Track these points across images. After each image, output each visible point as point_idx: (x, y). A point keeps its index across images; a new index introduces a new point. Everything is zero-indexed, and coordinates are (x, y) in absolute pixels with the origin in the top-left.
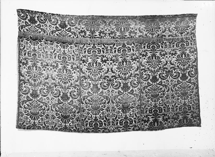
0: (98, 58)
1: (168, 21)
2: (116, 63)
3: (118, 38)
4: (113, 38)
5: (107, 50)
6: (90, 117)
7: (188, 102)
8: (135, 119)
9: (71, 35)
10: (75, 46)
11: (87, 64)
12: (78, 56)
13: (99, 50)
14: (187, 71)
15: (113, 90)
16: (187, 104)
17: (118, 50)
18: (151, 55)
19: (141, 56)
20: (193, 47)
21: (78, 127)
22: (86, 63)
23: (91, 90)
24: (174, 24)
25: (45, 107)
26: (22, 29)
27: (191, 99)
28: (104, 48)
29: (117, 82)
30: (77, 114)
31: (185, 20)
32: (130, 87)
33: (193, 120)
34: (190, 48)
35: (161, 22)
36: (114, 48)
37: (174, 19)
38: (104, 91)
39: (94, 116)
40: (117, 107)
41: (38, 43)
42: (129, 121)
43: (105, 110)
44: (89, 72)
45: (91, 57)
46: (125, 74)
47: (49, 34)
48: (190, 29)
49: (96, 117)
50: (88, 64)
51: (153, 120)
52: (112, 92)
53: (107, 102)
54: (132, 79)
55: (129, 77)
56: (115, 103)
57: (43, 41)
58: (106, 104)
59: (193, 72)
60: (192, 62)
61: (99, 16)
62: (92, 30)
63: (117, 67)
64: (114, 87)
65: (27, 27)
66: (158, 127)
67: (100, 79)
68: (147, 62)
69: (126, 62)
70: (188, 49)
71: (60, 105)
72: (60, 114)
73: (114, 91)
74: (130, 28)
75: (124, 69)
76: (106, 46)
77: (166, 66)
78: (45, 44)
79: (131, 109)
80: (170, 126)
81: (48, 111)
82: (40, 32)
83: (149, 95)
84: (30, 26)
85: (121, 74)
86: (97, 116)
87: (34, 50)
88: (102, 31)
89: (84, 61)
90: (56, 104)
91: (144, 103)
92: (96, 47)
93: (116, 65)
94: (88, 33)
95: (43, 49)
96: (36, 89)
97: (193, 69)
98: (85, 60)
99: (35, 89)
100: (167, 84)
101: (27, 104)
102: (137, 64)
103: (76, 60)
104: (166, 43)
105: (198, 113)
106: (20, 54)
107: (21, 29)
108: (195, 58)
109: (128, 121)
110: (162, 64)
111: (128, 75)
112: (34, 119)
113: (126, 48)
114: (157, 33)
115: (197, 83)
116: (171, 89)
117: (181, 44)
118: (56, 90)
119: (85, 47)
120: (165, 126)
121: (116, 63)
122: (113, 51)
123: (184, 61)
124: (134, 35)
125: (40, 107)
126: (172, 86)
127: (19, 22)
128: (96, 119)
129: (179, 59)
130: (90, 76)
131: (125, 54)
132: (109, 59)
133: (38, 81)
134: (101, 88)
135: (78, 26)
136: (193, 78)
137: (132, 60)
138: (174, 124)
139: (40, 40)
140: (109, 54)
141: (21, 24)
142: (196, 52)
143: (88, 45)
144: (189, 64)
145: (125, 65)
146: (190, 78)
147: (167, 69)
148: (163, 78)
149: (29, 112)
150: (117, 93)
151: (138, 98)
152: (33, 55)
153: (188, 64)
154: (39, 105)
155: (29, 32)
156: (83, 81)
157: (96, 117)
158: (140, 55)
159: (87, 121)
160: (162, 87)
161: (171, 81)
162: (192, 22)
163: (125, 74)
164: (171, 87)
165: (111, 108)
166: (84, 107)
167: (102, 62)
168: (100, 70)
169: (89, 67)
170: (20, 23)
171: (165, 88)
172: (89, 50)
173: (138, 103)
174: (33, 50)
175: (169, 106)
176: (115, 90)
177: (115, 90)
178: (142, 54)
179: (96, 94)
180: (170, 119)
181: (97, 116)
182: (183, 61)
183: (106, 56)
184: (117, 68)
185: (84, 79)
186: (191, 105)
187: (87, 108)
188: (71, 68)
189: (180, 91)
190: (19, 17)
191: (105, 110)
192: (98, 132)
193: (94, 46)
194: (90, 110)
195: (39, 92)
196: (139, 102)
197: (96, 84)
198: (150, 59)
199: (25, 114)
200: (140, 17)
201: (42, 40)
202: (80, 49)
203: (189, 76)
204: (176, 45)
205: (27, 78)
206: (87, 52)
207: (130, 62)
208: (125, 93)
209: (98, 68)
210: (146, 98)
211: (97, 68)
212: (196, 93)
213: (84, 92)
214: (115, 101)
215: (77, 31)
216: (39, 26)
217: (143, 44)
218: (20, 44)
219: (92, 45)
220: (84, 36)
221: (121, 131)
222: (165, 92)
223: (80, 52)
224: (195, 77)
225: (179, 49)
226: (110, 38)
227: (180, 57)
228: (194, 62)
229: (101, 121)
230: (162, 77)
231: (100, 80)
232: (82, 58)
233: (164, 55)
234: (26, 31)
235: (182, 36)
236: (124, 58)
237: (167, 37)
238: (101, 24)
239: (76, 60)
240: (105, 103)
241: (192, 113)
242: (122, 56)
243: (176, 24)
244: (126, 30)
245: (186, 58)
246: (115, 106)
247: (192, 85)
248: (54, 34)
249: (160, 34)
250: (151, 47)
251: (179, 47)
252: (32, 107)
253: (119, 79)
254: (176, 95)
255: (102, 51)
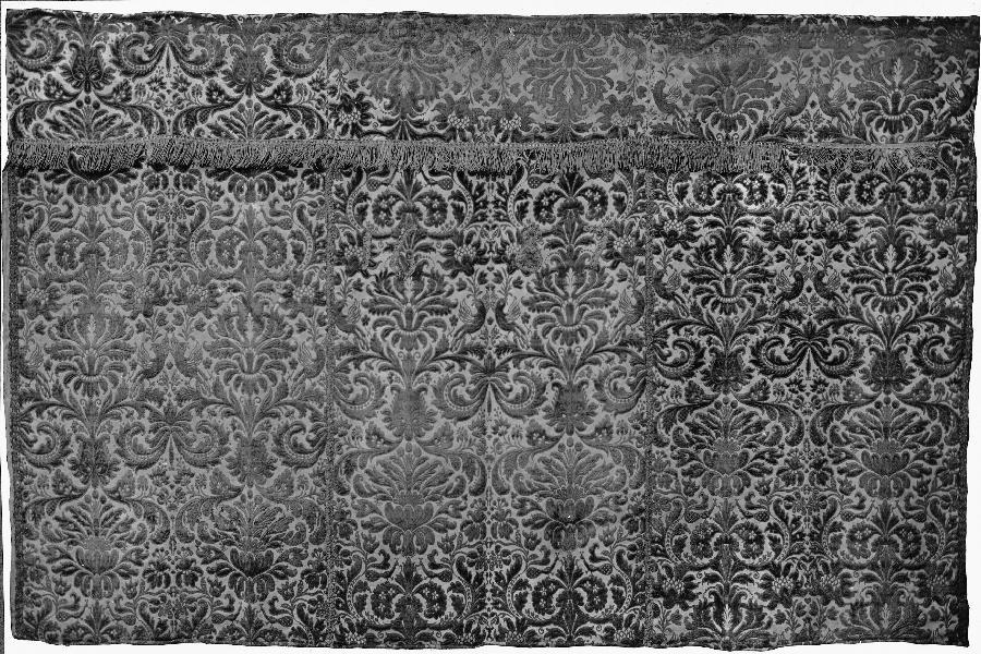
0: (427, 249)
1: (819, 51)
2: (523, 278)
3: (541, 139)
4: (516, 136)
5: (477, 207)
6: (378, 567)
7: (907, 508)
8: (617, 581)
9: (289, 126)
10: (309, 181)
11: (368, 282)
12: (323, 238)
13: (436, 204)
14: (908, 339)
15: (501, 423)
16: (901, 523)
17: (538, 207)
18: (713, 237)
19: (659, 241)
20: (954, 208)
21: (314, 616)
22: (366, 275)
23: (385, 420)
24: (852, 70)
25: (145, 522)
26: (27, 122)
27: (922, 493)
28: (465, 193)
29: (522, 381)
30: (312, 548)
31: (916, 53)
32: (596, 411)
33: (927, 610)
34: (932, 211)
35: (777, 59)
36: (516, 191)
37: (853, 41)
38: (456, 427)
39: (402, 560)
40: (520, 514)
41: (114, 190)
42: (584, 595)
43: (457, 530)
44: (376, 325)
45: (391, 240)
46: (570, 338)
47: (169, 127)
48: (941, 104)
49: (409, 567)
50: (373, 279)
51: (713, 237)
52: (495, 430)
53: (470, 485)
54: (604, 365)
55: (588, 358)
56: (513, 490)
57: (140, 172)
58: (465, 498)
59: (939, 350)
60: (940, 289)
61: (443, 16)
62: (404, 89)
63: (528, 296)
64: (509, 405)
65: (57, 108)
66: (737, 634)
67: (433, 360)
68: (691, 277)
69: (579, 269)
70: (923, 220)
71: (225, 503)
72: (227, 554)
73: (508, 427)
74: (607, 86)
75: (563, 311)
76: (475, 181)
77: (795, 304)
78: (151, 188)
79: (600, 530)
80: (804, 631)
81: (159, 546)
82: (124, 127)
83: (693, 457)
84: (73, 104)
85: (549, 336)
86: (415, 559)
87: (93, 230)
88: (457, 98)
89: (354, 266)
90: (203, 501)
91: (668, 501)
92: (417, 188)
93: (524, 285)
94: (379, 110)
95: (139, 215)
96: (98, 437)
97: (942, 329)
98: (361, 259)
99: (92, 437)
100: (790, 405)
101: (57, 519)
102: (636, 283)
103: (314, 261)
104: (801, 171)
105: (955, 571)
106: (21, 257)
107: (21, 126)
108: (956, 270)
109: (580, 590)
110: (772, 290)
111: (583, 343)
112: (96, 593)
113: (582, 193)
114: (754, 116)
115: (957, 411)
116: (813, 429)
117: (884, 185)
118: (202, 428)
119: (363, 188)
120: (779, 632)
121: (523, 278)
122: (512, 209)
123: (889, 280)
124: (629, 120)
125: (120, 528)
126: (818, 415)
127: (13, 86)
128: (409, 577)
129: (863, 271)
130: (384, 346)
131: (577, 225)
132: (487, 255)
133: (105, 391)
134: (440, 413)
135: (326, 72)
136: (938, 380)
137: (611, 258)
138: (821, 624)
139: (125, 170)
140: (488, 227)
141: (22, 98)
142: (964, 238)
143: (376, 178)
144: (920, 300)
145: (570, 289)
146: (926, 382)
147: (798, 316)
148: (775, 368)
149: (69, 557)
150: (525, 439)
151: (635, 471)
152: (86, 254)
153: (914, 298)
154: (116, 519)
155: (66, 136)
156: (348, 371)
157: (409, 567)
158: (657, 236)
159: (363, 586)
160: (765, 417)
161: (814, 388)
162: (951, 69)
163: (570, 338)
164: (810, 418)
165: (489, 518)
166: (350, 508)
167: (450, 272)
168: (437, 312)
169: (378, 296)
170: (18, 90)
171: (780, 424)
172: (384, 204)
173: (633, 500)
174: (84, 230)
175: (798, 525)
176: (511, 420)
177: (514, 422)
178: (667, 229)
179: (414, 443)
180: (802, 594)
181: (415, 559)
182: (883, 283)
183: (471, 235)
184: (526, 303)
185: (349, 361)
186: (920, 526)
187: (363, 516)
188: (285, 306)
189: (860, 447)
190: (12, 60)
191: (457, 530)
192: (421, 647)
193: (409, 182)
194: (379, 529)
195: (112, 446)
196: (642, 489)
197: (415, 388)
198: (709, 259)
199: (49, 567)
200: (661, 23)
201: (134, 171)
202: (335, 198)
203: (919, 369)
204: (860, 189)
205: (53, 378)
206: (370, 217)
207: (598, 270)
208: (566, 436)
209: (426, 300)
210: (680, 475)
211: (422, 303)
212: (953, 467)
213: (350, 431)
214: (510, 483)
215: (319, 102)
216: (122, 96)
217: (676, 175)
218: (20, 205)
219: (399, 177)
220: (356, 130)
221: (538, 641)
222: (782, 447)
223: (337, 216)
224: (952, 376)
225: (869, 213)
226: (497, 140)
227: (868, 260)
228: (951, 294)
229: (439, 590)
230: (770, 365)
231: (436, 369)
232: (343, 246)
233: (786, 240)
234: (51, 131)
235: (892, 141)
236: (571, 250)
237: (811, 141)
238: (452, 61)
239: (314, 261)
240: (458, 492)
241: (922, 571)
242: (558, 238)
243: (866, 73)
244: (585, 97)
245: (904, 267)
246: (510, 507)
247: (933, 417)
248: (200, 125)
249: (771, 122)
250: (715, 196)
251: (870, 201)
252: (83, 528)
253: (536, 362)
254: (835, 463)
255: (450, 209)
